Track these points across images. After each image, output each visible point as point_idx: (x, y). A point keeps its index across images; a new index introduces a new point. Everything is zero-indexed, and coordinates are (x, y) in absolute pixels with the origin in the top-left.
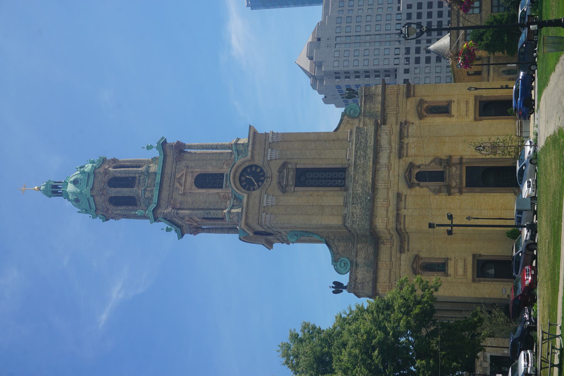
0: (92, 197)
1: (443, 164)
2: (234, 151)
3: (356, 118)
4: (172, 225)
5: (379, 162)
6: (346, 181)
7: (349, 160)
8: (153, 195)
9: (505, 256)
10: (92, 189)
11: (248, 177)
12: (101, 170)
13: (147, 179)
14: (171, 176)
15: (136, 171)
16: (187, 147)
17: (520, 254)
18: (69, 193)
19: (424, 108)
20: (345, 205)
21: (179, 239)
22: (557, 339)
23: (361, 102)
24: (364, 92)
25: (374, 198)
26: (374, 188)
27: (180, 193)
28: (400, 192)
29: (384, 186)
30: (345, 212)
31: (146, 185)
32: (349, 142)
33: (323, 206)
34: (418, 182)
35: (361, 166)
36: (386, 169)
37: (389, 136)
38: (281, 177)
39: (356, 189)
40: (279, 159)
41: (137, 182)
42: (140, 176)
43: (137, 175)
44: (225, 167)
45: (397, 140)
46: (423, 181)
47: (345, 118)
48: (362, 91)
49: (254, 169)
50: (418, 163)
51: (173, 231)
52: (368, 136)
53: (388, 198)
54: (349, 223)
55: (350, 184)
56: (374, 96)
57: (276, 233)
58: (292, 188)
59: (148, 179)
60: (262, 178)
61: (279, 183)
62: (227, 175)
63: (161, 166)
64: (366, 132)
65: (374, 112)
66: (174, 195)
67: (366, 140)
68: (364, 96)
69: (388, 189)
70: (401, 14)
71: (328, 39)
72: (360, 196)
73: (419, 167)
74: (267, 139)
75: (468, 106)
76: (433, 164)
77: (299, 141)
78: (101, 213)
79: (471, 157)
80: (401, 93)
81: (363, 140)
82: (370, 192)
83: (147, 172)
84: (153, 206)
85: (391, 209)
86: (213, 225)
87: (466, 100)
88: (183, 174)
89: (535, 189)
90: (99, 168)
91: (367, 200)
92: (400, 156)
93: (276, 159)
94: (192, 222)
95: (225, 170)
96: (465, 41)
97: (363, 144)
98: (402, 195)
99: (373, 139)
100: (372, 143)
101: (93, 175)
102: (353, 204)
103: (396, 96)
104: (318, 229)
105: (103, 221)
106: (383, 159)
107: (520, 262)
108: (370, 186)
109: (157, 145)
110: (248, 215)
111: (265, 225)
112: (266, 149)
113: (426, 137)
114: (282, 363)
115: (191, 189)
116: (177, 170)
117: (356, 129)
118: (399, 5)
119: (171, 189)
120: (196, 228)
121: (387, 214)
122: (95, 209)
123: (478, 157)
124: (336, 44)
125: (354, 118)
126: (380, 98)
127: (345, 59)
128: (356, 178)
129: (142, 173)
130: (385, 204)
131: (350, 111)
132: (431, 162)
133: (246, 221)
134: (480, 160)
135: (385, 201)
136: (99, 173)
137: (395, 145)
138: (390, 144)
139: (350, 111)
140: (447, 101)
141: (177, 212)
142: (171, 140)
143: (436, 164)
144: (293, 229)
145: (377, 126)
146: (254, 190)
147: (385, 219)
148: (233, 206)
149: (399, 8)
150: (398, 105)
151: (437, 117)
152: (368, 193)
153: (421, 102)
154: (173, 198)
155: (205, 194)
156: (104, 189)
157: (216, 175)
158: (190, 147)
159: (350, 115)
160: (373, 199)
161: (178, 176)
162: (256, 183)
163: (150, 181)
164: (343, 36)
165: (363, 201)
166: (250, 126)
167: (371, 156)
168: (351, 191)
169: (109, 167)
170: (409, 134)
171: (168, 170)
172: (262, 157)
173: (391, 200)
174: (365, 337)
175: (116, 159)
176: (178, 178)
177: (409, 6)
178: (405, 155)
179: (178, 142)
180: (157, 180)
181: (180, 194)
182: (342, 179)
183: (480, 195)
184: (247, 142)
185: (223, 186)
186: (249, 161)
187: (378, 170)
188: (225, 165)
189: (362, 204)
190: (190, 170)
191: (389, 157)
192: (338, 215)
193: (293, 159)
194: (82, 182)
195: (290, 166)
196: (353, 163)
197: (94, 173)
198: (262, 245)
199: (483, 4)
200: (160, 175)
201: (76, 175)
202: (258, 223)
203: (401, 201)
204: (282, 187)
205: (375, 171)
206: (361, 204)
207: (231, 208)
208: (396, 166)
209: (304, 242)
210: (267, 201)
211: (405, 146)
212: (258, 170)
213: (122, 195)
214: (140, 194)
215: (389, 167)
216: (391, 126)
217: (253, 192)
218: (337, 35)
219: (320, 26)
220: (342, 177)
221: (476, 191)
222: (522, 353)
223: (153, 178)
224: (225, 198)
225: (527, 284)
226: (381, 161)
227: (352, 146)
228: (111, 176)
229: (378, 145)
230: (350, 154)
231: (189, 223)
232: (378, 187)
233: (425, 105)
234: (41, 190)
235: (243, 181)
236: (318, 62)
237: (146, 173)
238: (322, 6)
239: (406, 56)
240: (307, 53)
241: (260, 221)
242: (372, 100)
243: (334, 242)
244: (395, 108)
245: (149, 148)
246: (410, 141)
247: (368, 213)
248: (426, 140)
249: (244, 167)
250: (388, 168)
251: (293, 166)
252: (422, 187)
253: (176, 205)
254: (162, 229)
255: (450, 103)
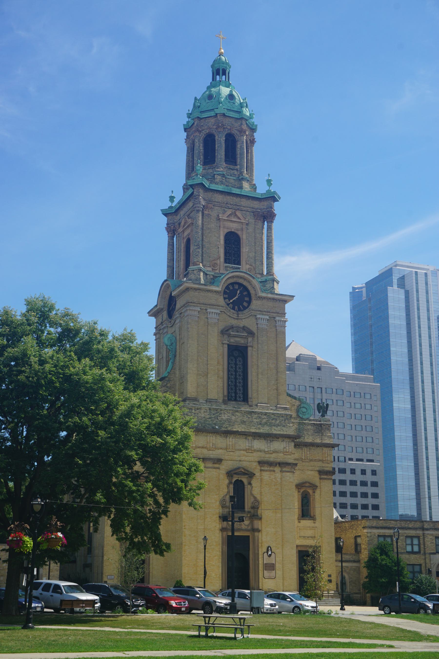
0: (215, 115)
1: (252, 511)
2: (265, 278)
3: (297, 414)
4: (180, 204)
5: (255, 439)
6: (233, 402)
7: (257, 405)
8: (217, 184)
9: (149, 579)
10: (224, 115)
11: (238, 292)
12: (244, 127)
13: (235, 178)
14: (238, 206)
15: (244, 165)
16: (270, 224)
17: (198, 596)
18: (218, 88)
19: (308, 490)
20: (208, 401)
21: (161, 210)
22: (241, 635)
23: (314, 420)
24: (325, 424)
25: (217, 433)
26: (227, 433)
27: (220, 215)
28: (223, 462)
29: (229, 445)
30: (201, 401)
31: (228, 177)
32: (276, 407)
33: (207, 376)
34: (233, 482)
35: (250, 419)
36: (247, 447)
37: (282, 450)
38: (238, 329)
39: (226, 413)
40: (258, 327)
41: (232, 167)
42: (237, 170)
43: (238, 167)
44: (248, 266)
45: (278, 460)
46: (234, 488)
47: (297, 401)
48: (326, 421)
49: (247, 299)
50: (253, 482)
51: (170, 204)
52: (282, 428)
53: (216, 448)
54: (189, 404)
55: (231, 406)
56: (321, 434)
57: (173, 322)
58: (226, 342)
59: (234, 180)
60: (236, 307)
61: (232, 327)
62: (239, 268)
63: (250, 195)
64: (287, 426)
65: (304, 434)
66: (217, 208)
67: (278, 425)
68: (321, 424)
69: (226, 449)
70: (345, 461)
71: (319, 379)
72: (219, 418)
73: (250, 484)
74: (279, 315)
75: (310, 538)
76: (252, 499)
77: (277, 351)
78: (195, 124)
79: (260, 541)
80: (324, 465)
81: (278, 422)
82: (223, 429)
83: (242, 178)
84: (206, 184)
85: (205, 451)
86: (177, 250)
87: (316, 536)
88: (241, 219)
89: (269, 612)
90: (246, 124)
91: (214, 425)
92: (261, 463)
93: (257, 324)
94: (184, 226)
95: (244, 266)
96: (378, 535)
97: (273, 421)
98: (219, 464)
99: (279, 433)
100: (275, 432)
101: (238, 117)
102: (210, 409)
103: (321, 459)
104: (179, 369)
105: (184, 125)
106: (258, 444)
107: (188, 595)
108: (229, 429)
109: (272, 191)
110: (198, 291)
111: (187, 310)
112: (269, 314)
113: (281, 492)
114: (114, 334)
115: (224, 227)
116: (244, 212)
117: (290, 415)
118: (354, 459)
119: (224, 205)
120: (174, 230)
121: (199, 447)
122: (200, 117)
123: (260, 550)
124: (313, 387)
125: (298, 411)
126: (318, 441)
127: (363, 405)
128: (237, 413)
129: (241, 173)
130: (210, 446)
131: (305, 408)
132: (255, 498)
133: (191, 288)
134: (257, 552)
135: (213, 446)
136: (242, 124)
137: (273, 457)
138: (275, 452)
139: (305, 408)
140: (315, 515)
141: (200, 210)
142: (277, 207)
143: (253, 503)
144: (180, 341)
145: (293, 438)
146: (225, 298)
147: (194, 445)
148: (206, 274)
149: (351, 459)
150: (311, 460)
151: (298, 504)
152: (222, 426)
153: (314, 487)
154: (214, 207)
155: (218, 243)
156: (224, 128)
157: (239, 256)
158: (270, 229)
159: (300, 408)
160: (214, 432)
161: (238, 213)
162: (231, 301)
163: (232, 181)
164: (322, 396)
165: (213, 421)
166: (293, 296)
167: (261, 430)
168: (223, 407)
169: (247, 135)
170: (284, 474)
171: (244, 202)
172: (260, 309)
173: (214, 452)
174: (170, 427)
175: (254, 143)
176: (235, 213)
177: (374, 473)
178: (262, 468)
179: (275, 216)
180: (235, 189)
181: (218, 215)
182: (236, 397)
183: (219, 551)
184: (276, 292)
185: (226, 263)
186: (256, 295)
187: (246, 438)
188: (250, 267)
189: (210, 420)
190: (244, 227)
191: (260, 451)
192: (197, 392)
193: (258, 343)
194: (232, 104)
195: (250, 339)
196: (253, 410)
197: (242, 118)
198: (156, 304)
199: (416, 556)
200: (240, 193)
201: (239, 98)
202: (189, 303)
203: (214, 463)
204: (227, 331)
205: (246, 435)
206: (210, 418)
207: (204, 272)
208: (250, 458)
209: (157, 352)
210: (212, 312)
211: (271, 468)
212: (245, 304)
213: (216, 148)
214: (219, 170)
215: (249, 450)
216: (293, 454)
217: (222, 297)
218: (324, 390)
219: (334, 371)
220: (238, 398)
221: (224, 547)
222: (96, 598)
223: (235, 185)
224: (214, 266)
225: (170, 603)
226: (256, 441)
227: (271, 409)
228: (237, 137)
229: (273, 438)
230: (263, 408)
231: (182, 224)
232: (228, 438)
233: (310, 491)
234: (220, 56)
235: (233, 287)
236: (294, 366)
237: (242, 177)
238: (352, 373)
239: (337, 470)
240: (304, 355)
241: (191, 304)
242: (316, 433)
243: (164, 387)
244: (308, 458)
245: (269, 182)
246: (277, 474)
247: (200, 425)
248: (278, 492)
249: (250, 288)
250: (249, 449)
251: (250, 343)
252: (228, 487)
253: (207, 210)
254: (172, 191)
255: (313, 518)
